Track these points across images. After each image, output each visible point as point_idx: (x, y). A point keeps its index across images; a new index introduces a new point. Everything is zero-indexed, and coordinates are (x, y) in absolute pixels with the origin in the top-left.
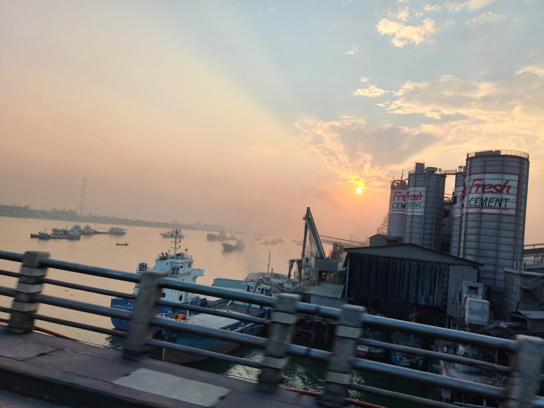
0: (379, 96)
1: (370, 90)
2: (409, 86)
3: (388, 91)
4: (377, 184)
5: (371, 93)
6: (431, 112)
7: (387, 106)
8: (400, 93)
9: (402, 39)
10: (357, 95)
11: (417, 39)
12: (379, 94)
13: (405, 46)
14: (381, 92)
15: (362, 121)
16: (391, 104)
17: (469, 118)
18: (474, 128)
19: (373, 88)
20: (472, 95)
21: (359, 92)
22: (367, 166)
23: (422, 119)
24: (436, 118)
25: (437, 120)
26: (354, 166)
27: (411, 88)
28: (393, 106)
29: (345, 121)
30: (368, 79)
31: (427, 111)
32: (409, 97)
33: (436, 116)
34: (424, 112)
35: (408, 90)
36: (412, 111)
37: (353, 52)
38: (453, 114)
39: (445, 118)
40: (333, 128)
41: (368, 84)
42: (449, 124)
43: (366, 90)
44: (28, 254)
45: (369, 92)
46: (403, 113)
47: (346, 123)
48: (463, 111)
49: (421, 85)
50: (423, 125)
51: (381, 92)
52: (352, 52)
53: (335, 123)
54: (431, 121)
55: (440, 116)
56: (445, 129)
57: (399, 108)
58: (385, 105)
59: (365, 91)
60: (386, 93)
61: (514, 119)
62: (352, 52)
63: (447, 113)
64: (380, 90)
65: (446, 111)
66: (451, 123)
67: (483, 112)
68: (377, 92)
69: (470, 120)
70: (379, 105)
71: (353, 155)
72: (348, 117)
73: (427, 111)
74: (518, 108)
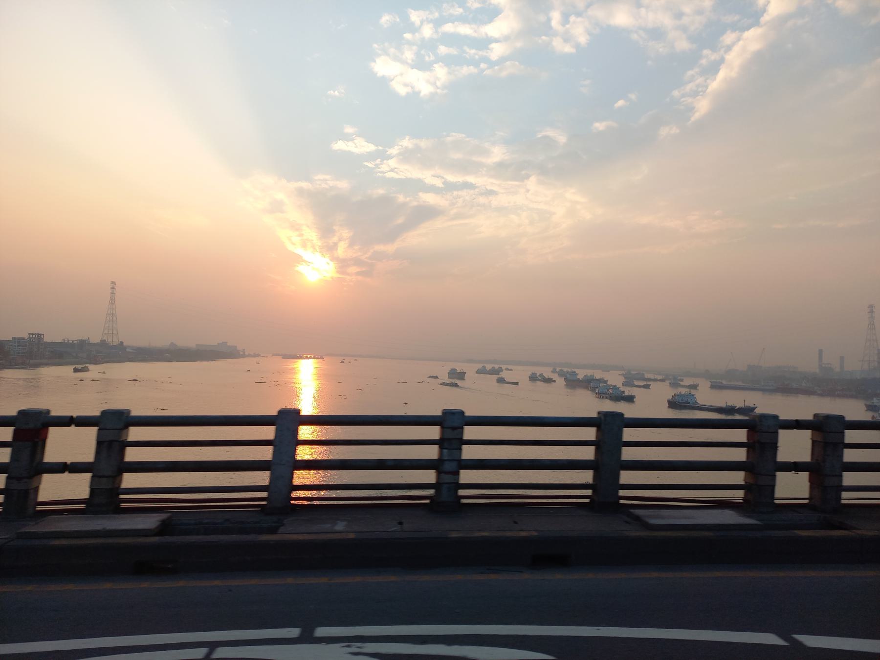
2: (407, 143)
4: (353, 269)
5: (356, 147)
6: (433, 177)
7: (377, 166)
8: (394, 151)
9: (406, 85)
13: (408, 93)
14: (371, 148)
15: (343, 185)
16: (382, 164)
18: (482, 200)
19: (360, 141)
23: (420, 186)
27: (410, 146)
28: (384, 168)
32: (407, 156)
33: (439, 183)
36: (409, 175)
37: (338, 92)
38: (459, 182)
39: (450, 187)
40: (300, 192)
41: (355, 136)
42: (453, 194)
43: (350, 143)
47: (320, 185)
48: (471, 179)
49: (423, 144)
50: (421, 194)
51: (371, 148)
52: (336, 92)
53: (304, 185)
54: (432, 189)
55: (443, 183)
56: (447, 200)
57: (392, 170)
58: (374, 165)
61: (528, 191)
62: (336, 92)
64: (370, 145)
65: (451, 178)
66: (455, 193)
68: (361, 146)
69: (477, 190)
70: (366, 164)
71: (326, 231)
73: (428, 176)
74: (533, 179)
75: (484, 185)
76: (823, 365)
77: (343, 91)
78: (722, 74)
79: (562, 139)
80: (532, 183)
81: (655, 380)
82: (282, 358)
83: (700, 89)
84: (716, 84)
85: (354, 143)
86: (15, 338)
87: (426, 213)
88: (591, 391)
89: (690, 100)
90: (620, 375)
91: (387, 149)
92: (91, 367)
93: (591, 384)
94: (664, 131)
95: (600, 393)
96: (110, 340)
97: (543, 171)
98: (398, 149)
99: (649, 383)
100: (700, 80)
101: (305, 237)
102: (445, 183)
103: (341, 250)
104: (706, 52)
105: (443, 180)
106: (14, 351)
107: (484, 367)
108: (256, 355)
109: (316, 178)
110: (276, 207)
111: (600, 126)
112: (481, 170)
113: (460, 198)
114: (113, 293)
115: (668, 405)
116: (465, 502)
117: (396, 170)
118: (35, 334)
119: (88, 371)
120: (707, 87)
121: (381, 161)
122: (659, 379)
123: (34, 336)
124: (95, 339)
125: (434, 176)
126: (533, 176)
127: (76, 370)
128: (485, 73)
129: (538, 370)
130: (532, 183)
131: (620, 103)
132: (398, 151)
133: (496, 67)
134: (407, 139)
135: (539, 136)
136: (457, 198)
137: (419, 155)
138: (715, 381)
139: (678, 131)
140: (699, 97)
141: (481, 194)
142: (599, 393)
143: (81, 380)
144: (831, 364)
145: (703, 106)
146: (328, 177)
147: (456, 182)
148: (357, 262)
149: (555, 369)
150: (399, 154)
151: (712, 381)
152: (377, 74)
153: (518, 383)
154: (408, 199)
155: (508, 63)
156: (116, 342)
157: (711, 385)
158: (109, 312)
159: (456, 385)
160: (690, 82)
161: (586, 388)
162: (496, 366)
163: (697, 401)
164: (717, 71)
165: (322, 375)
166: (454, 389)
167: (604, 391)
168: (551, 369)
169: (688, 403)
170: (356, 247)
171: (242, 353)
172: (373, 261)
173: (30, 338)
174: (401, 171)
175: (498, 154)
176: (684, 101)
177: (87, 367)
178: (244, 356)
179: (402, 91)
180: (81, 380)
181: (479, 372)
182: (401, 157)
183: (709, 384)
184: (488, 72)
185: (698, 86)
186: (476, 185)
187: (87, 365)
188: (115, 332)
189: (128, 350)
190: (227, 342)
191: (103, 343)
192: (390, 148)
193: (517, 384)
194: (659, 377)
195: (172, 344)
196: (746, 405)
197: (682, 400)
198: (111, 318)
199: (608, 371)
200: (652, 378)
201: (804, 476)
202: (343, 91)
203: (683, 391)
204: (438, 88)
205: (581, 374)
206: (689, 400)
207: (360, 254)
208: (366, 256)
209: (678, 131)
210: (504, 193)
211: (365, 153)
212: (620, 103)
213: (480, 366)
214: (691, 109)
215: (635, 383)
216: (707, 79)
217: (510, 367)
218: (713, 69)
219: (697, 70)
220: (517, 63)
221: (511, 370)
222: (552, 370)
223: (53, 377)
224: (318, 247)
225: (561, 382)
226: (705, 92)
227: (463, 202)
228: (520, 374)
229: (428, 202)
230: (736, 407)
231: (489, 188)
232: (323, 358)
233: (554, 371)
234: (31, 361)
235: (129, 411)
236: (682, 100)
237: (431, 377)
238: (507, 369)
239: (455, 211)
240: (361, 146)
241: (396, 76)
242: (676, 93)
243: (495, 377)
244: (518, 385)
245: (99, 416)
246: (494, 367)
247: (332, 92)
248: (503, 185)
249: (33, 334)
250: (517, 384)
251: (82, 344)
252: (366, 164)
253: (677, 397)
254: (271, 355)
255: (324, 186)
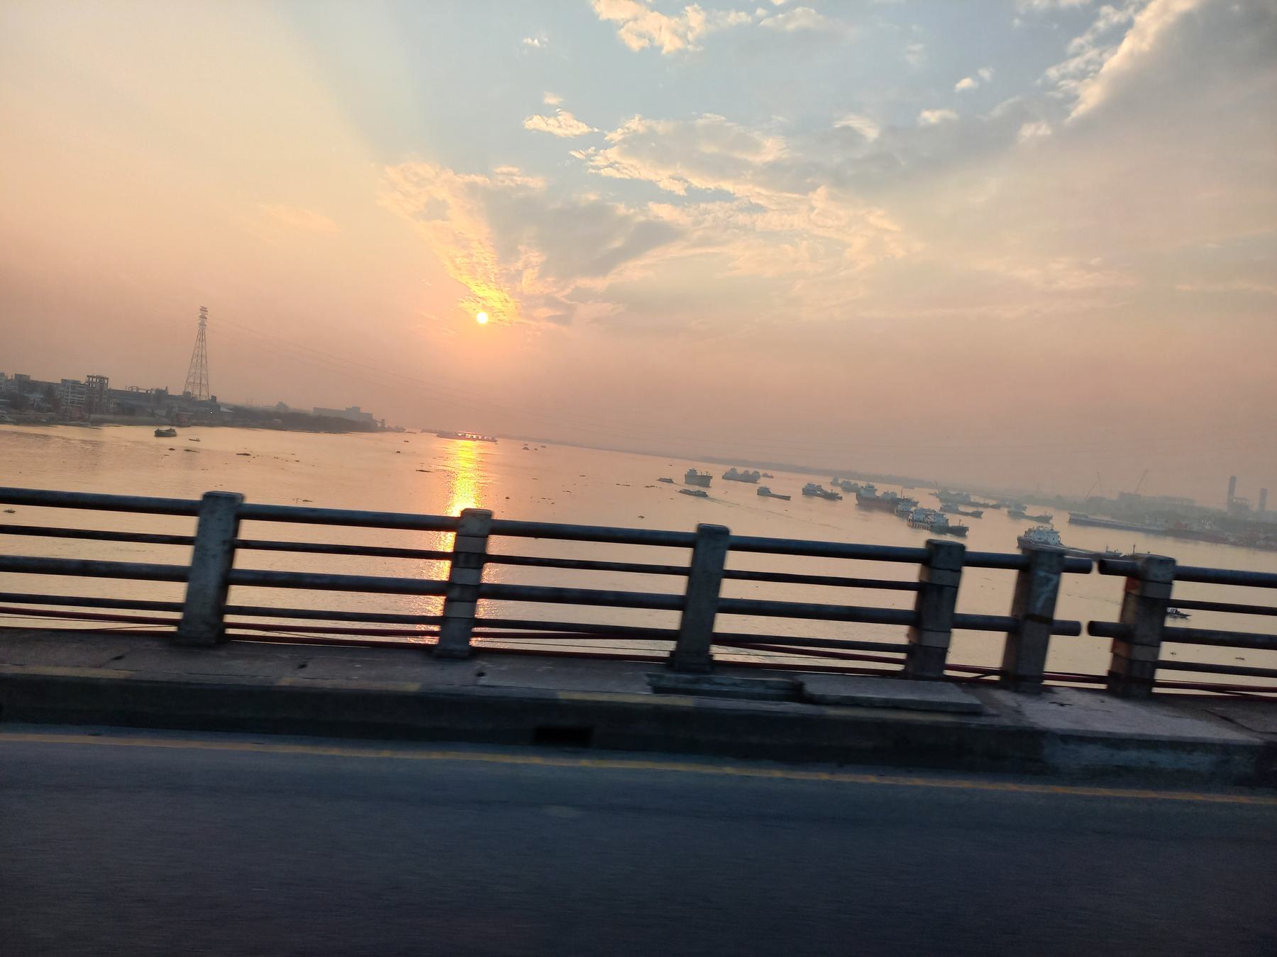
0: (576, 136)
1: (559, 122)
2: (635, 124)
3: (596, 130)
4: (544, 312)
5: (560, 127)
6: (671, 180)
7: (589, 157)
8: (616, 136)
9: (641, 36)
10: (532, 127)
11: (669, 43)
12: (577, 132)
13: (643, 48)
14: (584, 129)
15: (537, 183)
16: (596, 155)
17: (737, 199)
18: (742, 218)
19: (565, 117)
20: (750, 158)
21: (536, 123)
22: (529, 275)
23: (648, 192)
24: (677, 193)
25: (678, 196)
26: (504, 271)
27: (641, 129)
28: (599, 161)
29: (500, 177)
30: (561, 100)
31: (664, 179)
32: (634, 145)
33: (679, 189)
34: (658, 179)
35: (635, 131)
36: (636, 174)
37: (539, 41)
38: (710, 189)
39: (695, 196)
40: (472, 189)
41: (558, 110)
42: (699, 207)
43: (551, 121)
44: (210, 497)
45: (558, 125)
46: (618, 175)
47: (503, 182)
48: (728, 186)
49: (661, 127)
50: (651, 204)
51: (584, 129)
52: (536, 41)
53: (479, 179)
54: (670, 198)
55: (685, 190)
56: (690, 216)
57: (611, 165)
58: (586, 156)
59: (548, 122)
60: (593, 133)
61: (812, 209)
62: (536, 41)
63: (699, 186)
64: (580, 124)
65: (697, 182)
66: (703, 206)
67: (763, 191)
68: (567, 126)
69: (736, 203)
70: (573, 153)
71: (507, 252)
72: (511, 169)
73: (664, 179)
74: (822, 191)
75: (747, 197)
76: (1235, 501)
77: (546, 40)
78: (1127, 45)
79: (872, 133)
80: (819, 198)
81: (986, 506)
82: (438, 436)
83: (1091, 68)
84: (1116, 60)
85: (557, 120)
86: (66, 380)
87: (656, 235)
88: (897, 515)
89: (1073, 84)
90: (931, 494)
91: (606, 132)
92: (178, 430)
93: (899, 506)
94: (1028, 131)
95: (916, 521)
96: (197, 392)
97: (839, 180)
98: (624, 133)
99: (980, 509)
100: (1092, 53)
101: (475, 260)
102: (689, 189)
103: (528, 284)
104: (1106, 9)
105: (686, 185)
106: (67, 399)
107: (733, 470)
108: (399, 430)
109: (498, 170)
110: (435, 210)
111: (931, 117)
112: (745, 172)
113: (709, 214)
114: (202, 324)
115: (1017, 545)
116: (487, 628)
117: (617, 165)
118: (97, 377)
119: (175, 436)
120: (1101, 65)
121: (595, 151)
122: (991, 504)
123: (95, 380)
124: (176, 390)
125: (673, 179)
126: (823, 187)
127: (159, 434)
128: (762, 23)
129: (816, 480)
130: (819, 198)
131: (966, 83)
132: (621, 137)
133: (780, 16)
134: (637, 118)
135: (837, 126)
136: (705, 214)
137: (653, 144)
138: (1077, 513)
139: (1049, 132)
140: (1087, 80)
141: (741, 210)
142: (913, 521)
143: (171, 449)
144: (1246, 500)
145: (1092, 95)
146: (515, 170)
147: (706, 189)
148: (551, 302)
149: (836, 480)
150: (623, 141)
151: (1073, 512)
152: (598, 16)
153: (790, 497)
154: (632, 211)
155: (799, 10)
156: (204, 396)
157: (1070, 519)
158: (196, 351)
159: (704, 495)
160: (1076, 55)
161: (891, 511)
162: (751, 471)
163: (1061, 542)
164: (1120, 40)
165: (483, 464)
166: (702, 500)
167: (922, 517)
168: (830, 479)
169: (1048, 544)
170: (550, 279)
171: (379, 425)
172: (573, 303)
173: (88, 382)
174: (624, 168)
175: (772, 149)
176: (1063, 85)
177: (174, 431)
178: (383, 429)
179: (635, 44)
180: (171, 449)
181: (727, 477)
182: (626, 146)
183: (1068, 517)
184: (767, 22)
185: (1088, 62)
186: (735, 196)
187: (174, 428)
188: (204, 382)
189: (223, 409)
190: (359, 408)
191: (187, 397)
192: (610, 131)
193: (788, 498)
194: (992, 502)
195: (281, 405)
196: (1136, 552)
197: (1040, 539)
198: (199, 361)
199: (913, 488)
200: (982, 502)
201: (1000, 637)
202: (546, 40)
203: (1034, 525)
204: (689, 42)
205: (881, 490)
206: (1050, 540)
207: (554, 289)
208: (565, 293)
209: (1049, 132)
210: (777, 210)
211: (573, 137)
212: (966, 83)
213: (728, 468)
214: (1072, 98)
215: (959, 508)
216: (1104, 51)
217: (769, 473)
218: (1115, 36)
219: (1088, 37)
220: (813, 11)
221: (772, 477)
222: (831, 481)
223: (130, 441)
224: (493, 275)
225: (850, 499)
226: (1097, 72)
227: (713, 221)
228: (791, 484)
229: (662, 217)
230: (1121, 554)
231: (754, 201)
232: (496, 441)
233: (834, 483)
234: (91, 415)
235: (242, 497)
236: (1061, 83)
237: (661, 480)
238: (765, 475)
239: (700, 233)
240: (567, 126)
241: (628, 21)
242: (1053, 73)
243: (753, 488)
244: (789, 500)
245: (200, 501)
246: (748, 471)
247: (530, 41)
248: (775, 198)
249: (93, 377)
250: (788, 498)
251: (160, 397)
252: (573, 153)
253: (1032, 534)
254: (420, 430)
255: (508, 182)
